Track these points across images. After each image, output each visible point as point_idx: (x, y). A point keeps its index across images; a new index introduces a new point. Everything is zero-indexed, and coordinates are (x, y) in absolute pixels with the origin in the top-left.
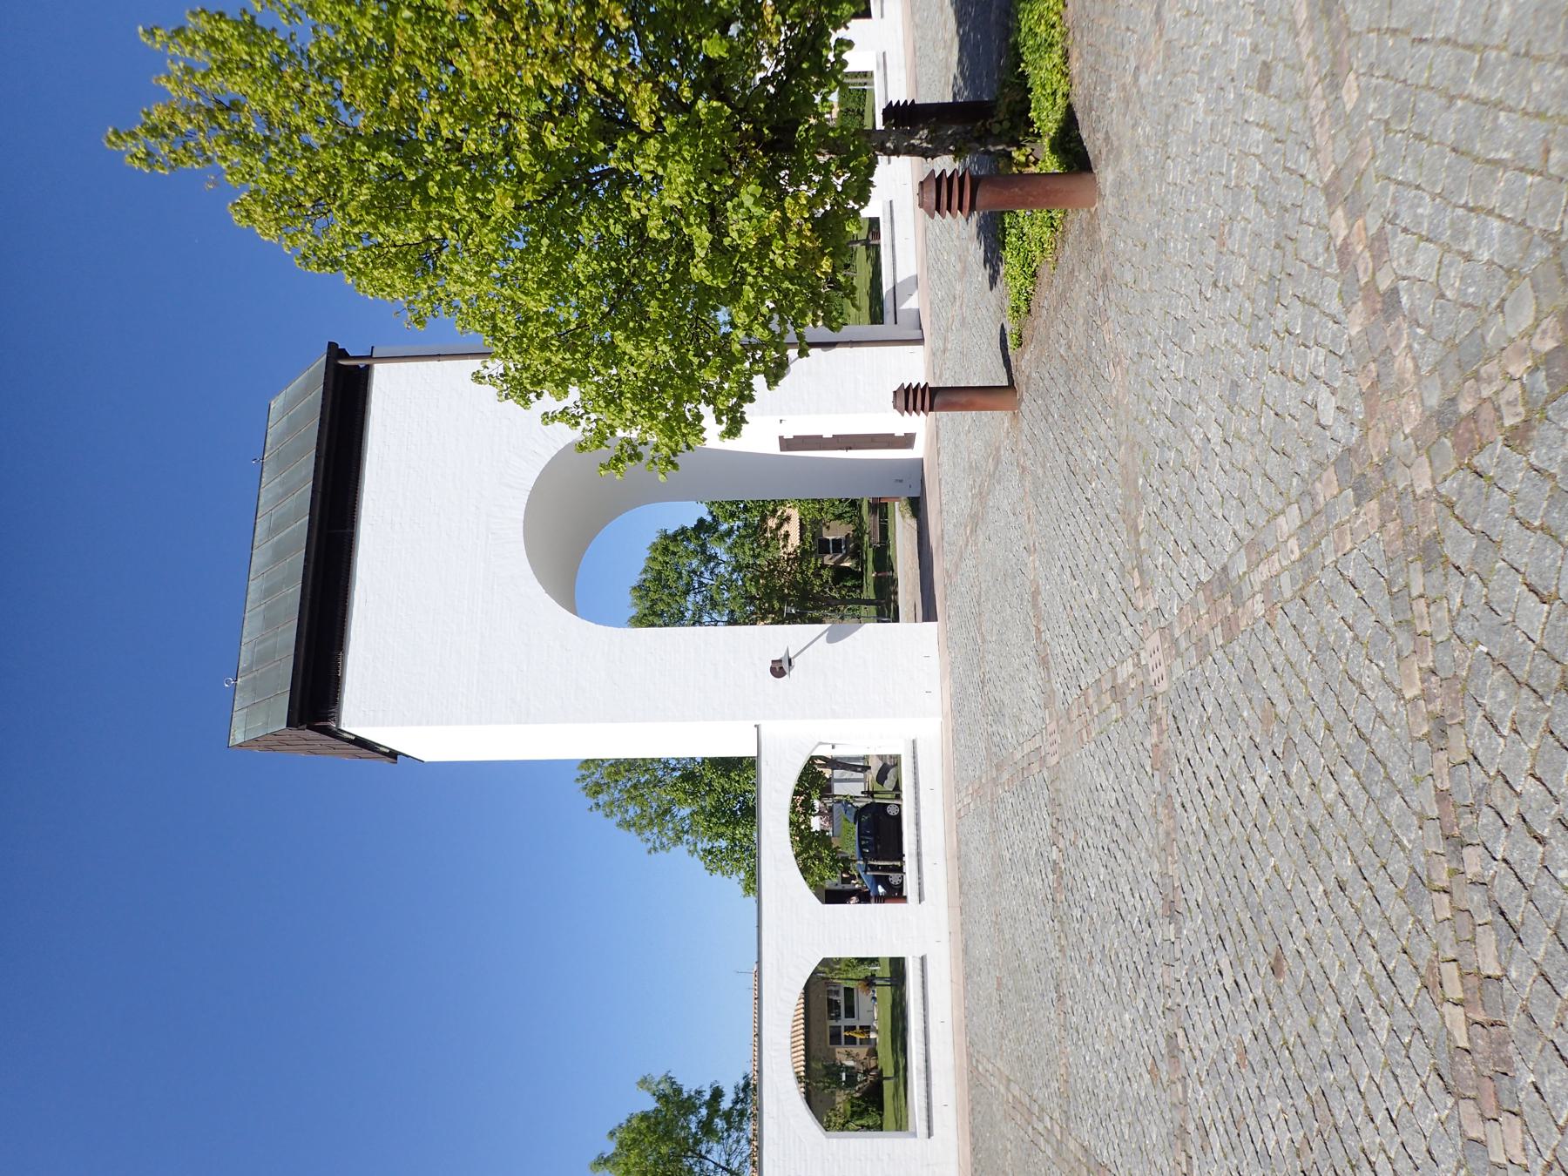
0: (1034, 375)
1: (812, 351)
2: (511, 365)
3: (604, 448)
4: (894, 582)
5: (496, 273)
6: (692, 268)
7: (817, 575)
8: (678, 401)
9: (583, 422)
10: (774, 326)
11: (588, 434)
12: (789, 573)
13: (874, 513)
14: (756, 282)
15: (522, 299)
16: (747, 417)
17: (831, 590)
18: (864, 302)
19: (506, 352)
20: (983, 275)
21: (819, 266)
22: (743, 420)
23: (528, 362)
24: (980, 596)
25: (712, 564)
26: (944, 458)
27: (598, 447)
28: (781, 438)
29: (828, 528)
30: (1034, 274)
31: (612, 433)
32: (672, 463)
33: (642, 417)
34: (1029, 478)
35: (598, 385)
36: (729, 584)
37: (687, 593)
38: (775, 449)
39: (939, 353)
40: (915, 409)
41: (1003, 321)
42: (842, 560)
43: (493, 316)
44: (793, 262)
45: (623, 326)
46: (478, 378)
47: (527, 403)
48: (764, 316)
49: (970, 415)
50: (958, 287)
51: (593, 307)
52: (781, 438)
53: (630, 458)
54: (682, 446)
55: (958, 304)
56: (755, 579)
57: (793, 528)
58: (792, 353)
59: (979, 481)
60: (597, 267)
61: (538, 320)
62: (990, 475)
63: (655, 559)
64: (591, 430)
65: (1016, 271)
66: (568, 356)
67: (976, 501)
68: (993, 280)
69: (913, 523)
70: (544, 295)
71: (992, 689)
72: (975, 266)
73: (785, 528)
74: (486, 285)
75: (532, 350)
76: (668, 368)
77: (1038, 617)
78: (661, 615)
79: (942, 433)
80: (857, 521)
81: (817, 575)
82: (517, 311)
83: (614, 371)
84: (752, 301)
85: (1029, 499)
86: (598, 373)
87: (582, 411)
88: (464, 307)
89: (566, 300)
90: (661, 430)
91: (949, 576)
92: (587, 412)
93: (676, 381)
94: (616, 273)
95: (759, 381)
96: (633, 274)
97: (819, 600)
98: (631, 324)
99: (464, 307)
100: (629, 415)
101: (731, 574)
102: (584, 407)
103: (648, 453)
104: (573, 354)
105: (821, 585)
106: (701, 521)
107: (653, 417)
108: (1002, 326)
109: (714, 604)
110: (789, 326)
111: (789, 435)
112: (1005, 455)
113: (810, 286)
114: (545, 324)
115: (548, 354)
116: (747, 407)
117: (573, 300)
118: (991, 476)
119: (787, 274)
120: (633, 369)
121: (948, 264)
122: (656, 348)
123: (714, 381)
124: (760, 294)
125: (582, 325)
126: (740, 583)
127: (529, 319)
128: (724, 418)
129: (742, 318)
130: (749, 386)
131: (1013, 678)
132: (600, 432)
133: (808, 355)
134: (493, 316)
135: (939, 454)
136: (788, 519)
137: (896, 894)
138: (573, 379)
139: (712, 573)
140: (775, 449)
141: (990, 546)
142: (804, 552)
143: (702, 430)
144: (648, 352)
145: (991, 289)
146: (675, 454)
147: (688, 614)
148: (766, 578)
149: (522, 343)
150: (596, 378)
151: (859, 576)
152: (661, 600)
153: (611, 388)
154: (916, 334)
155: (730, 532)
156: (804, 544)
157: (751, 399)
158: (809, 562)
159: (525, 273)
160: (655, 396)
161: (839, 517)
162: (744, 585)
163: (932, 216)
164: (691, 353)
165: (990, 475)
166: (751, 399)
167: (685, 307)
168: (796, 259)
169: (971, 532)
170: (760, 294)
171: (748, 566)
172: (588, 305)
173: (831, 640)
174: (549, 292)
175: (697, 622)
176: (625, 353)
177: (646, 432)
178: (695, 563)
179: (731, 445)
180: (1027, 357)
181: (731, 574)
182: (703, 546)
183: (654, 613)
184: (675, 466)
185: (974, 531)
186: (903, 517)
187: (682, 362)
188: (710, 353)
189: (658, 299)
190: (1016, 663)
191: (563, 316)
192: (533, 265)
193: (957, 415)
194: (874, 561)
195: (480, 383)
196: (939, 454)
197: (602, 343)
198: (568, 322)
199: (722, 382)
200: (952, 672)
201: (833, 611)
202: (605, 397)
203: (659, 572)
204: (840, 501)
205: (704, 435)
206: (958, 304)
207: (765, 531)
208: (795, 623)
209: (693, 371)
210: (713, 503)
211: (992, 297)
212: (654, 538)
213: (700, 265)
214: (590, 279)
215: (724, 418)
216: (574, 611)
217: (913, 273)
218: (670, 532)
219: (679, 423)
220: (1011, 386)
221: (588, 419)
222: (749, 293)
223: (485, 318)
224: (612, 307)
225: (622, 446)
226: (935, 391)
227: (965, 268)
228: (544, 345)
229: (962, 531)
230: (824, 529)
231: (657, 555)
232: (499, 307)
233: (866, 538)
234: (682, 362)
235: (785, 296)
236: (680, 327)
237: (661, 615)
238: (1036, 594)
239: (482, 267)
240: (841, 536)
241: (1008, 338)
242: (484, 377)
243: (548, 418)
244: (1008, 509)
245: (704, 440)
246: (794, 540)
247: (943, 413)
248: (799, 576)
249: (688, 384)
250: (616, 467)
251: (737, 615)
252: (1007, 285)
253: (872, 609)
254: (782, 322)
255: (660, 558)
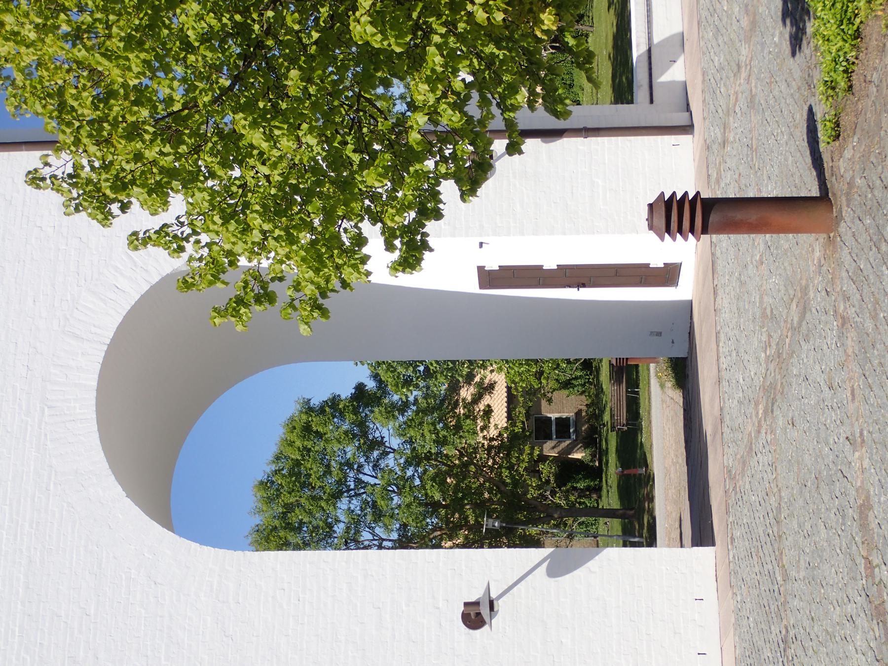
0: (859, 181)
1: (530, 145)
2: (85, 162)
3: (219, 285)
4: (649, 479)
5: (65, 28)
6: (352, 25)
7: (533, 471)
8: (329, 217)
9: (189, 247)
10: (473, 109)
11: (196, 264)
12: (491, 468)
13: (619, 381)
14: (446, 43)
15: (103, 64)
16: (431, 241)
17: (553, 493)
18: (604, 69)
19: (77, 142)
20: (780, 34)
21: (538, 22)
22: (425, 246)
23: (110, 158)
24: (779, 508)
25: (376, 453)
26: (724, 301)
27: (211, 283)
28: (481, 269)
29: (550, 401)
30: (857, 35)
31: (232, 263)
32: (319, 307)
33: (275, 239)
34: (852, 334)
35: (213, 193)
36: (402, 484)
37: (336, 496)
38: (471, 285)
39: (715, 147)
40: (680, 231)
41: (812, 101)
42: (570, 449)
43: (61, 92)
44: (499, 17)
45: (248, 107)
46: (35, 179)
47: (106, 218)
48: (458, 94)
49: (761, 240)
50: (744, 51)
51: (208, 78)
52: (481, 269)
53: (258, 300)
54: (335, 283)
55: (744, 75)
56: (439, 479)
57: (498, 401)
58: (499, 145)
59: (776, 336)
60: (214, 22)
61: (126, 97)
62: (793, 329)
63: (291, 444)
64: (200, 259)
65: (831, 29)
66: (167, 149)
67: (772, 367)
68: (796, 42)
69: (677, 396)
70: (135, 59)
71: (800, 652)
72: (769, 21)
73: (486, 400)
74: (53, 47)
75: (115, 139)
76: (315, 169)
77: (869, 543)
78: (299, 529)
79: (720, 264)
80: (593, 391)
81: (533, 471)
82: (96, 84)
83: (237, 173)
84: (439, 69)
85: (854, 366)
86: (212, 175)
87: (188, 231)
88: (19, 78)
89: (167, 69)
90: (303, 260)
91: (732, 478)
92: (195, 233)
93: (327, 188)
94: (242, 30)
95: (448, 189)
96: (268, 32)
97: (535, 509)
98: (261, 104)
99: (19, 78)
100: (256, 236)
101: (404, 469)
102: (191, 224)
103: (283, 292)
104: (175, 147)
105: (539, 487)
106: (360, 388)
107: (292, 240)
108: (810, 110)
109: (378, 515)
110: (495, 110)
111: (493, 265)
112: (817, 300)
113: (526, 51)
114: (136, 103)
115: (139, 145)
116: (431, 226)
117: (179, 70)
118: (796, 329)
119: (492, 34)
120: (265, 170)
121: (729, 17)
122: (298, 139)
123: (383, 187)
124: (452, 60)
125: (191, 105)
126: (417, 482)
127: (111, 94)
128: (397, 242)
129: (423, 93)
130: (435, 195)
131: (831, 636)
132: (214, 261)
133: (520, 152)
134: (61, 92)
135: (715, 293)
136: (491, 387)
137: (631, 102)
138: (176, 184)
139: (375, 466)
140: (471, 285)
141: (794, 434)
142: (514, 437)
143: (365, 259)
144: (287, 144)
145: (794, 54)
146: (323, 295)
147: (339, 529)
148: (455, 476)
149: (102, 129)
150: (210, 183)
151: (596, 473)
152: (299, 505)
153: (231, 196)
154: (680, 119)
155: (404, 407)
156: (513, 424)
157: (438, 215)
158: (521, 452)
159: (109, 27)
160: (296, 209)
161: (566, 385)
162: (423, 487)
163: (662, 239)
164: (350, 147)
165: (793, 329)
166: (438, 215)
167: (341, 80)
168: (505, 11)
169: (765, 412)
170: (452, 60)
171: (428, 457)
172: (200, 77)
173: (553, 572)
174: (143, 55)
175: (352, 541)
176: (252, 146)
177: (281, 262)
178: (350, 450)
179: (406, 280)
180: (848, 154)
181: (404, 469)
182: (362, 425)
183: (289, 527)
184: (324, 312)
185: (769, 411)
186: (662, 386)
187: (337, 160)
188: (377, 147)
189: (300, 68)
190: (836, 614)
191: (164, 92)
192: (120, 15)
193: (744, 239)
194: (618, 451)
195: (38, 187)
196: (715, 293)
197: (220, 133)
198: (169, 100)
199: (394, 190)
200: (737, 625)
201: (556, 526)
202: (222, 211)
203: (297, 463)
204: (568, 362)
205: (369, 266)
206: (744, 75)
207: (456, 404)
208: (498, 546)
209: (352, 173)
210: (379, 364)
211: (796, 65)
212: (291, 409)
213: (363, 19)
214: (206, 38)
215: (397, 242)
216: (167, 522)
217: (677, 28)
218: (316, 402)
219: (330, 249)
220: (824, 198)
221: (198, 242)
222: (435, 59)
223: (50, 96)
224: (236, 79)
225: (246, 283)
226: (710, 205)
227: (754, 24)
228: (134, 132)
229: (751, 410)
230: (544, 403)
231: (293, 437)
232: (70, 77)
233: (606, 417)
234: (337, 160)
235: (488, 67)
236: (333, 110)
237: (299, 529)
238: (865, 508)
239: (47, 18)
240: (568, 413)
241: (820, 127)
242: (43, 179)
243: (137, 240)
244: (821, 379)
245: (368, 274)
246: (499, 418)
247: (723, 237)
248: (505, 473)
249: (343, 191)
250: (236, 314)
251: (412, 529)
252: (817, 48)
253: (616, 525)
254: (484, 102)
255: (298, 443)
